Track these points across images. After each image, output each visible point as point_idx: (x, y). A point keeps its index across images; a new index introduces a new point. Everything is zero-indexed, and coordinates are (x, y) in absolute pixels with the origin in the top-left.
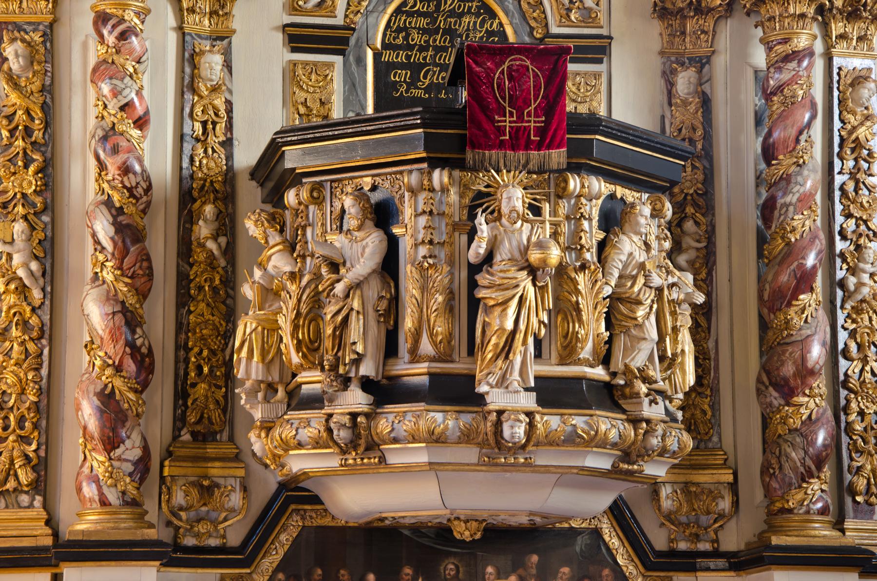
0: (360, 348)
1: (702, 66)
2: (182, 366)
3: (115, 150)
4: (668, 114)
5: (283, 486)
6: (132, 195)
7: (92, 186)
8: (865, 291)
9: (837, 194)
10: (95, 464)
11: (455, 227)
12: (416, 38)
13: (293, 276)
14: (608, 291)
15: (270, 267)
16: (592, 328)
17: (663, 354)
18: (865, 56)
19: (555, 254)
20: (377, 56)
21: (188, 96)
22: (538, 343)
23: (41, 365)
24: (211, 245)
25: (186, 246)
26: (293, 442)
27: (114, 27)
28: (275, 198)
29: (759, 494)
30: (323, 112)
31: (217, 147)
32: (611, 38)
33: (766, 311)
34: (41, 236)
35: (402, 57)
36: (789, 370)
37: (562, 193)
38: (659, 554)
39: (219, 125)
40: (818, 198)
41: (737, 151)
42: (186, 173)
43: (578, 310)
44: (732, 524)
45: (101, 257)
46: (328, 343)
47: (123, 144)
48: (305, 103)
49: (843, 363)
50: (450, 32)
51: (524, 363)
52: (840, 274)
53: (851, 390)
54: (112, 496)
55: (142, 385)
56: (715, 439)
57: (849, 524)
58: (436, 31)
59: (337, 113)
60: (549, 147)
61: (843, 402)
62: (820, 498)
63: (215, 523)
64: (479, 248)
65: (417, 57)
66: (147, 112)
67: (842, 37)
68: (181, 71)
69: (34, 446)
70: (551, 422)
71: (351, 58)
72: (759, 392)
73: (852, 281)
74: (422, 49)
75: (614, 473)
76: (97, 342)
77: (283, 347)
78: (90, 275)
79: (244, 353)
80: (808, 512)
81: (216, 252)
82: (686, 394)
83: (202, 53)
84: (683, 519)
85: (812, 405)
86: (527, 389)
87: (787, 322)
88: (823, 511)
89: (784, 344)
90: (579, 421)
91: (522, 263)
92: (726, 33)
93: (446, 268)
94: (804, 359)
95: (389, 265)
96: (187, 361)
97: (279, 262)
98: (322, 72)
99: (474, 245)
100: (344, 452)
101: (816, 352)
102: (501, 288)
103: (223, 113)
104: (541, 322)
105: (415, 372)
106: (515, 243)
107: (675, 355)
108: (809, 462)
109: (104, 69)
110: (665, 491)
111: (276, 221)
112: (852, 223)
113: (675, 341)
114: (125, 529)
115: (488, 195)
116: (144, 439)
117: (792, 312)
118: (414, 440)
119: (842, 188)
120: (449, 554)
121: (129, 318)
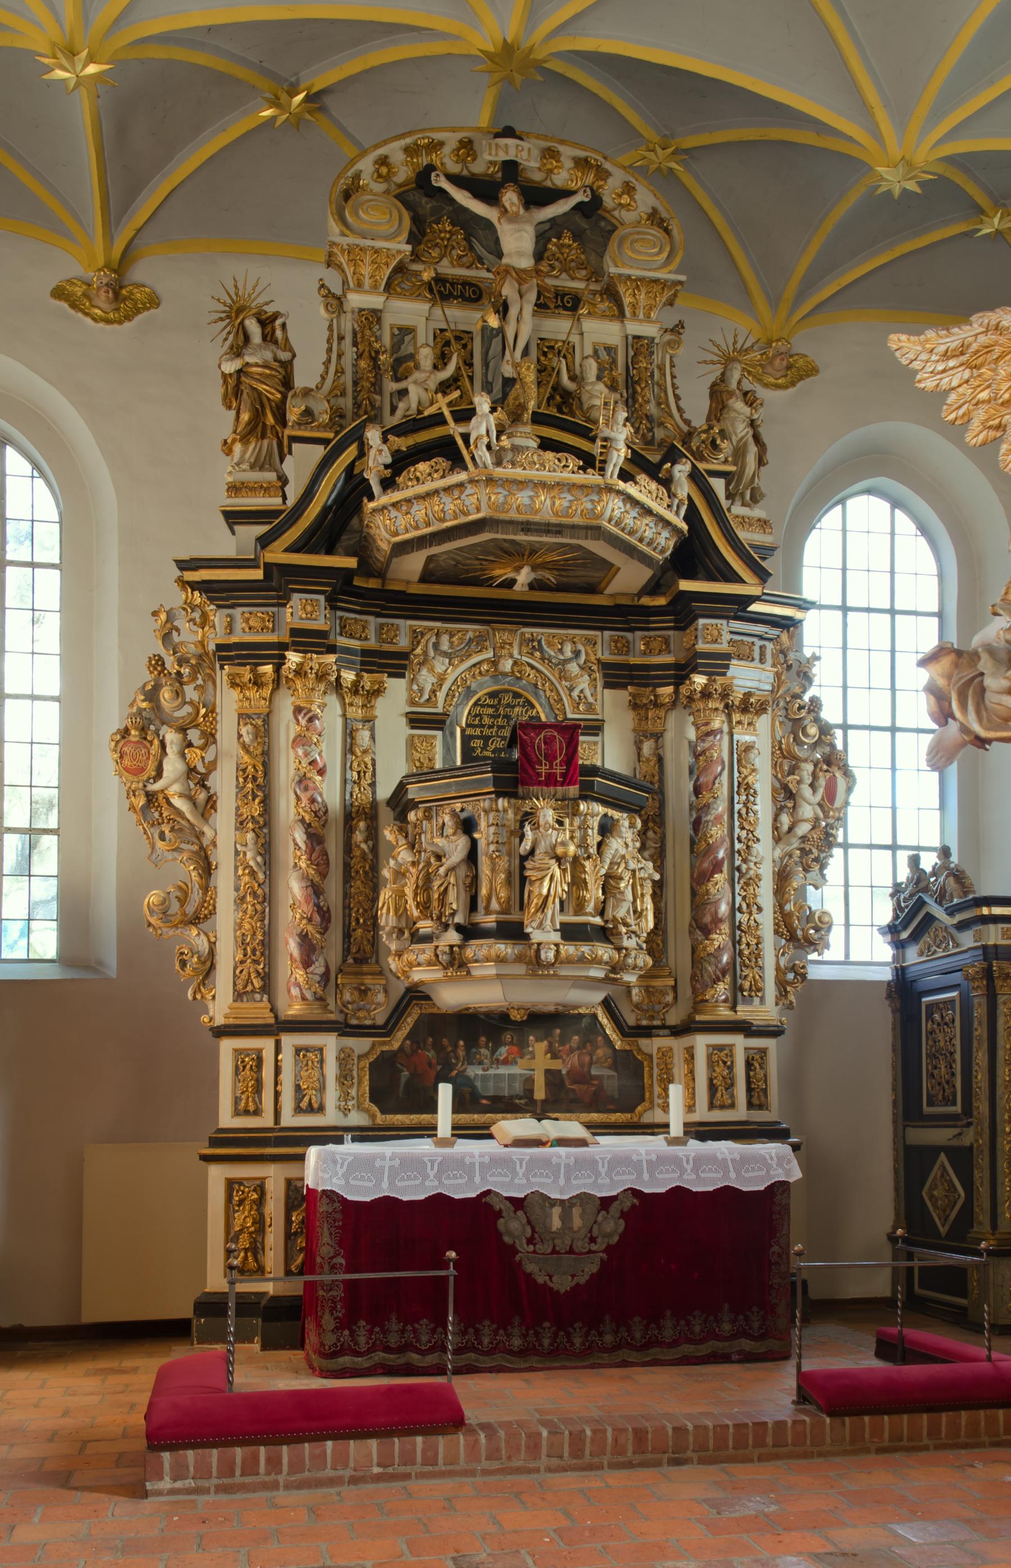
0: (454, 906)
1: (658, 738)
2: (347, 919)
3: (306, 789)
4: (638, 768)
5: (408, 990)
6: (316, 816)
7: (293, 811)
8: (752, 872)
9: (736, 815)
10: (298, 976)
11: (512, 833)
12: (487, 721)
13: (413, 864)
14: (603, 872)
15: (399, 859)
16: (594, 893)
17: (636, 913)
18: (752, 735)
19: (572, 849)
20: (463, 731)
21: (349, 756)
22: (562, 902)
23: (264, 918)
24: (363, 846)
25: (348, 847)
26: (415, 963)
27: (305, 715)
28: (402, 817)
29: (689, 992)
30: (430, 765)
31: (366, 787)
32: (603, 721)
33: (695, 884)
34: (263, 841)
35: (478, 732)
36: (707, 919)
37: (576, 813)
38: (631, 1028)
39: (368, 774)
40: (726, 817)
41: (679, 789)
42: (348, 803)
43: (586, 883)
44: (673, 1010)
45: (298, 853)
46: (435, 904)
47: (311, 785)
48: (419, 760)
49: (738, 915)
50: (507, 717)
51: (553, 915)
52: (737, 863)
53: (742, 931)
54: (308, 995)
55: (324, 930)
56: (664, 960)
57: (739, 1008)
58: (499, 716)
59: (438, 765)
60: (569, 784)
61: (738, 938)
62: (724, 994)
63: (369, 1011)
64: (527, 845)
65: (487, 732)
66: (325, 766)
67: (739, 722)
68: (345, 741)
69: (262, 966)
70: (569, 949)
71: (447, 733)
72: (690, 933)
73: (744, 867)
74: (490, 727)
75: (607, 980)
76: (297, 904)
77: (408, 906)
78: (292, 864)
79: (384, 911)
80: (717, 1001)
81: (366, 850)
82: (648, 934)
83: (357, 730)
84: (645, 1007)
85: (720, 939)
86: (555, 930)
87: (707, 891)
88: (725, 1001)
89: (706, 904)
90: (585, 949)
91: (552, 855)
92: (672, 719)
93: (507, 858)
94: (716, 912)
95: (472, 857)
96: (350, 915)
97: (405, 856)
98: (429, 740)
99: (523, 844)
100: (445, 968)
101: (724, 909)
102: (540, 869)
103: (370, 766)
104: (563, 890)
105: (488, 921)
106: (548, 843)
107: (642, 910)
108: (718, 973)
109: (300, 740)
110: (635, 991)
111: (402, 830)
112: (744, 832)
113: (642, 902)
114: (316, 1014)
115: (532, 814)
116: (326, 962)
117: (710, 884)
118: (488, 961)
119: (739, 813)
120: (507, 1029)
121: (316, 890)
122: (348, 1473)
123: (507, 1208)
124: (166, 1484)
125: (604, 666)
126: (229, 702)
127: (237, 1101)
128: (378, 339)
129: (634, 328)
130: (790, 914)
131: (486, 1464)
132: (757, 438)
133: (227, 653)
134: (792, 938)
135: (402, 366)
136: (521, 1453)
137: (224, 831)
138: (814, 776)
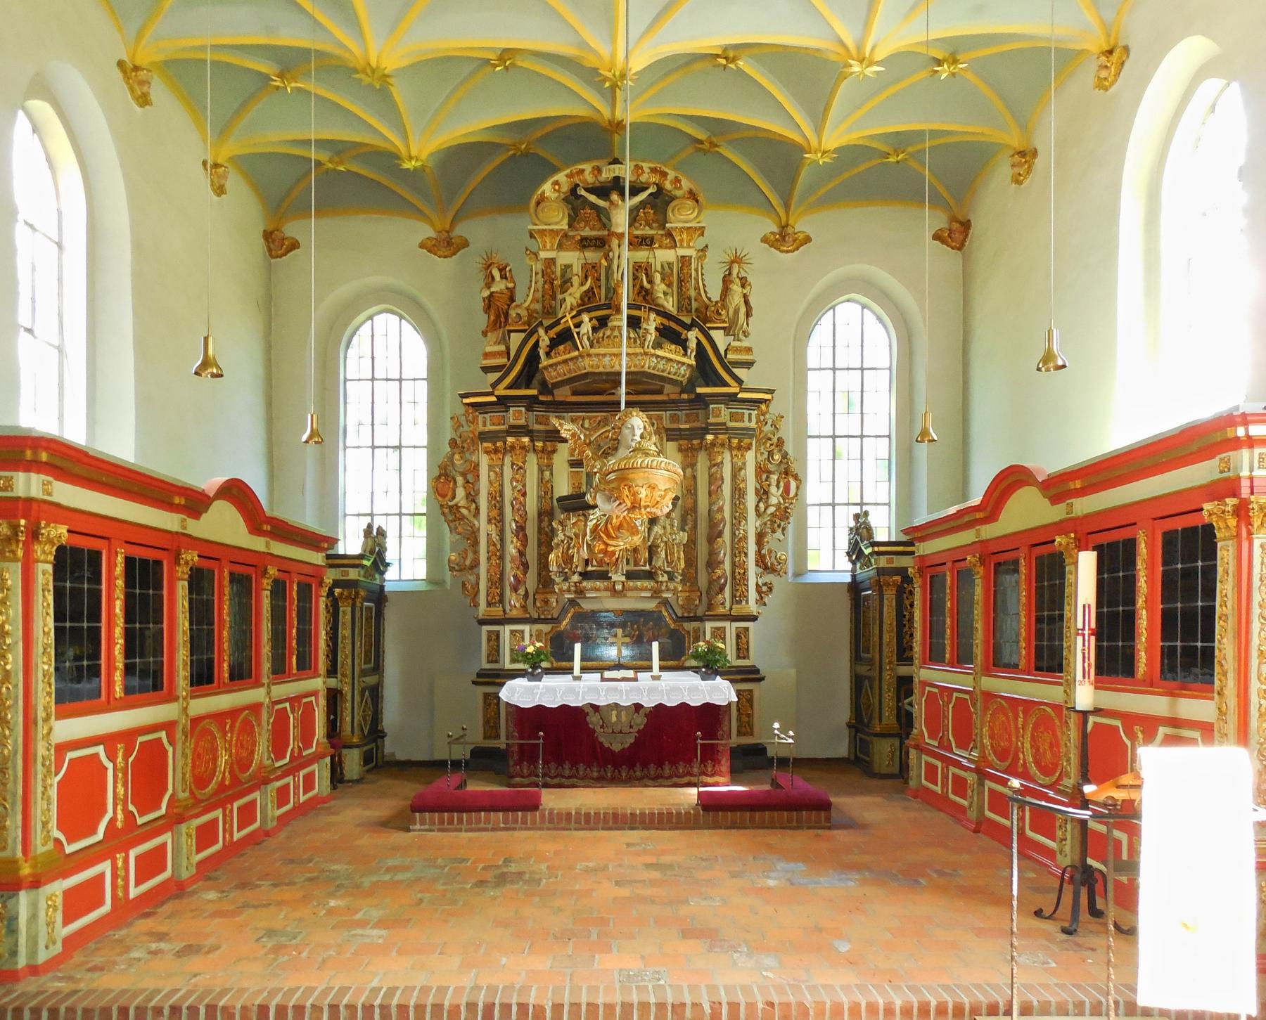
55: (525, 573)
122: (490, 826)
123: (590, 710)
124: (418, 827)
125: (667, 430)
126: (484, 461)
127: (488, 656)
128: (554, 273)
129: (681, 252)
130: (765, 555)
131: (548, 825)
132: (747, 303)
133: (484, 437)
134: (766, 568)
135: (566, 283)
136: (564, 821)
137: (484, 527)
138: (778, 482)
